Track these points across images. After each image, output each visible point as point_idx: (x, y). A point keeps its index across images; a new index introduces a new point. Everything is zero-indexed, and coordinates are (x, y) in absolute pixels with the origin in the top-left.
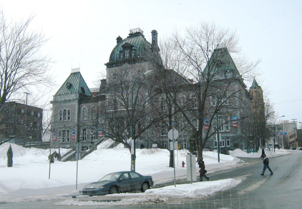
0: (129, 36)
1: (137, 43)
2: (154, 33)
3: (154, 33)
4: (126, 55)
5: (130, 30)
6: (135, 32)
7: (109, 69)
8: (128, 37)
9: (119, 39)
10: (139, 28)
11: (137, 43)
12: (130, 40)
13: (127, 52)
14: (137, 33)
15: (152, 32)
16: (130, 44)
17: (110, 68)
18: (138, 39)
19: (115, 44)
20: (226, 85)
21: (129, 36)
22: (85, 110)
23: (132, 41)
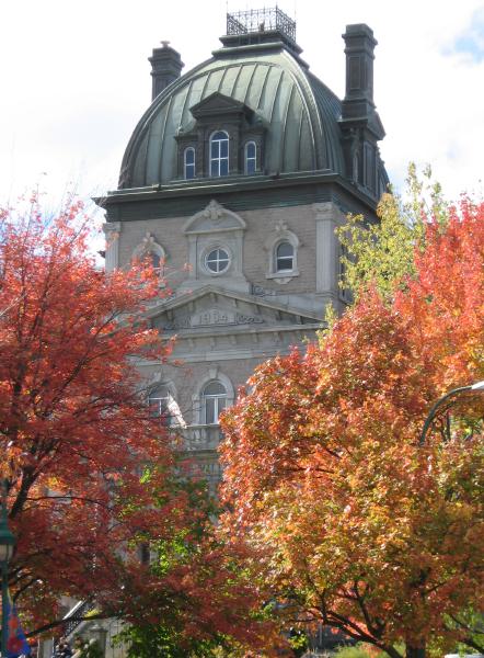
0: (219, 46)
1: (268, 103)
2: (359, 42)
3: (359, 42)
4: (211, 160)
5: (228, 17)
6: (252, 26)
7: (118, 225)
8: (218, 56)
9: (165, 63)
10: (278, 12)
11: (268, 103)
12: (233, 72)
13: (221, 139)
14: (263, 36)
15: (153, 61)
16: (230, 100)
17: (128, 225)
18: (262, 70)
19: (140, 96)
20: (363, 626)
21: (219, 46)
22: (216, 398)
23: (243, 81)
